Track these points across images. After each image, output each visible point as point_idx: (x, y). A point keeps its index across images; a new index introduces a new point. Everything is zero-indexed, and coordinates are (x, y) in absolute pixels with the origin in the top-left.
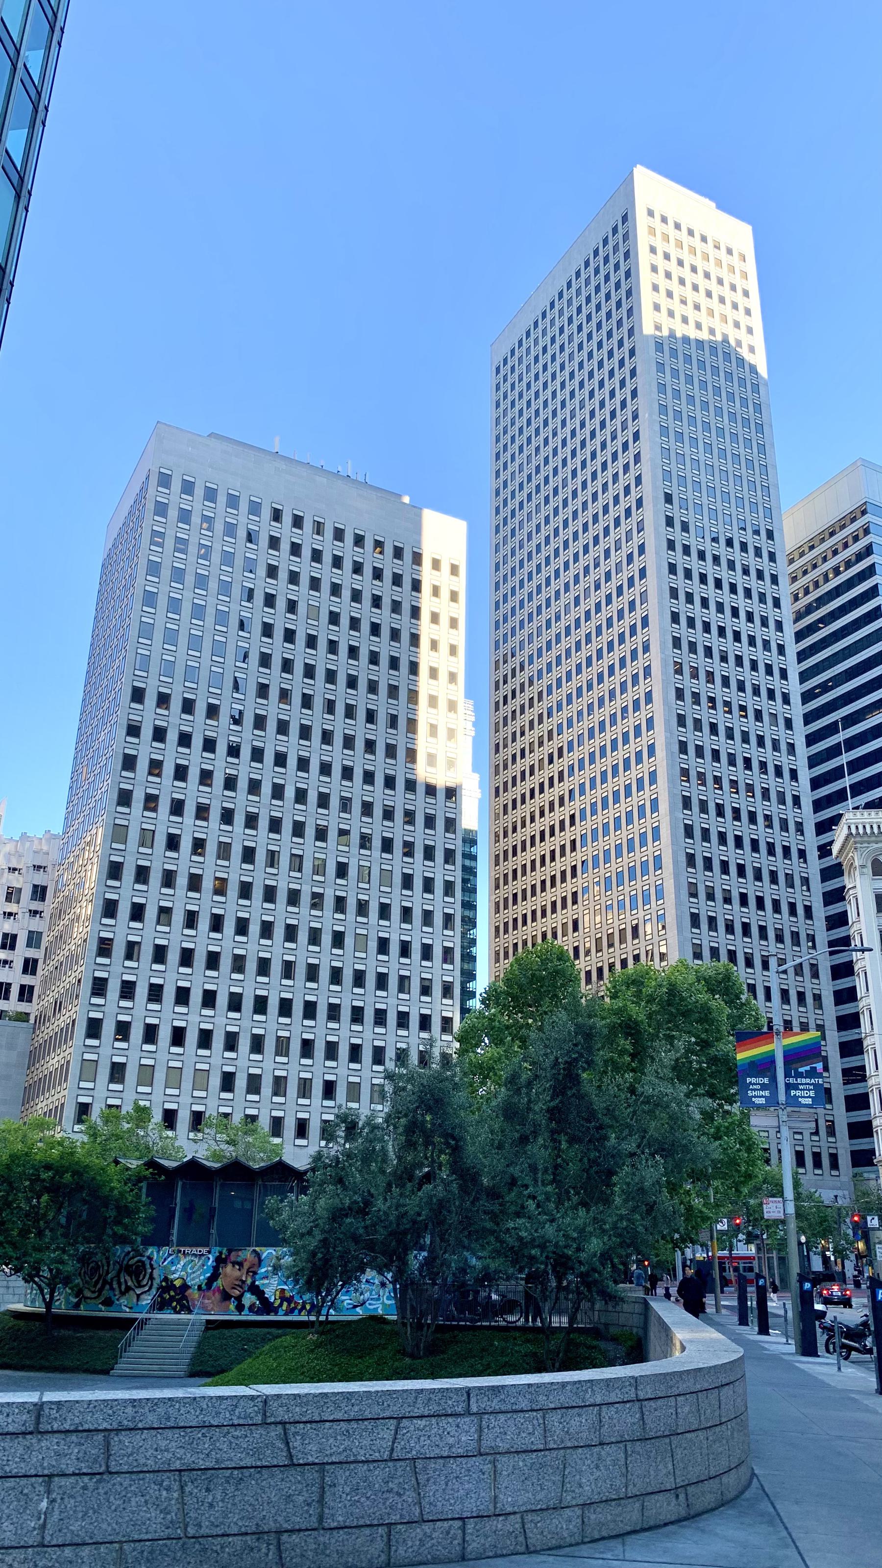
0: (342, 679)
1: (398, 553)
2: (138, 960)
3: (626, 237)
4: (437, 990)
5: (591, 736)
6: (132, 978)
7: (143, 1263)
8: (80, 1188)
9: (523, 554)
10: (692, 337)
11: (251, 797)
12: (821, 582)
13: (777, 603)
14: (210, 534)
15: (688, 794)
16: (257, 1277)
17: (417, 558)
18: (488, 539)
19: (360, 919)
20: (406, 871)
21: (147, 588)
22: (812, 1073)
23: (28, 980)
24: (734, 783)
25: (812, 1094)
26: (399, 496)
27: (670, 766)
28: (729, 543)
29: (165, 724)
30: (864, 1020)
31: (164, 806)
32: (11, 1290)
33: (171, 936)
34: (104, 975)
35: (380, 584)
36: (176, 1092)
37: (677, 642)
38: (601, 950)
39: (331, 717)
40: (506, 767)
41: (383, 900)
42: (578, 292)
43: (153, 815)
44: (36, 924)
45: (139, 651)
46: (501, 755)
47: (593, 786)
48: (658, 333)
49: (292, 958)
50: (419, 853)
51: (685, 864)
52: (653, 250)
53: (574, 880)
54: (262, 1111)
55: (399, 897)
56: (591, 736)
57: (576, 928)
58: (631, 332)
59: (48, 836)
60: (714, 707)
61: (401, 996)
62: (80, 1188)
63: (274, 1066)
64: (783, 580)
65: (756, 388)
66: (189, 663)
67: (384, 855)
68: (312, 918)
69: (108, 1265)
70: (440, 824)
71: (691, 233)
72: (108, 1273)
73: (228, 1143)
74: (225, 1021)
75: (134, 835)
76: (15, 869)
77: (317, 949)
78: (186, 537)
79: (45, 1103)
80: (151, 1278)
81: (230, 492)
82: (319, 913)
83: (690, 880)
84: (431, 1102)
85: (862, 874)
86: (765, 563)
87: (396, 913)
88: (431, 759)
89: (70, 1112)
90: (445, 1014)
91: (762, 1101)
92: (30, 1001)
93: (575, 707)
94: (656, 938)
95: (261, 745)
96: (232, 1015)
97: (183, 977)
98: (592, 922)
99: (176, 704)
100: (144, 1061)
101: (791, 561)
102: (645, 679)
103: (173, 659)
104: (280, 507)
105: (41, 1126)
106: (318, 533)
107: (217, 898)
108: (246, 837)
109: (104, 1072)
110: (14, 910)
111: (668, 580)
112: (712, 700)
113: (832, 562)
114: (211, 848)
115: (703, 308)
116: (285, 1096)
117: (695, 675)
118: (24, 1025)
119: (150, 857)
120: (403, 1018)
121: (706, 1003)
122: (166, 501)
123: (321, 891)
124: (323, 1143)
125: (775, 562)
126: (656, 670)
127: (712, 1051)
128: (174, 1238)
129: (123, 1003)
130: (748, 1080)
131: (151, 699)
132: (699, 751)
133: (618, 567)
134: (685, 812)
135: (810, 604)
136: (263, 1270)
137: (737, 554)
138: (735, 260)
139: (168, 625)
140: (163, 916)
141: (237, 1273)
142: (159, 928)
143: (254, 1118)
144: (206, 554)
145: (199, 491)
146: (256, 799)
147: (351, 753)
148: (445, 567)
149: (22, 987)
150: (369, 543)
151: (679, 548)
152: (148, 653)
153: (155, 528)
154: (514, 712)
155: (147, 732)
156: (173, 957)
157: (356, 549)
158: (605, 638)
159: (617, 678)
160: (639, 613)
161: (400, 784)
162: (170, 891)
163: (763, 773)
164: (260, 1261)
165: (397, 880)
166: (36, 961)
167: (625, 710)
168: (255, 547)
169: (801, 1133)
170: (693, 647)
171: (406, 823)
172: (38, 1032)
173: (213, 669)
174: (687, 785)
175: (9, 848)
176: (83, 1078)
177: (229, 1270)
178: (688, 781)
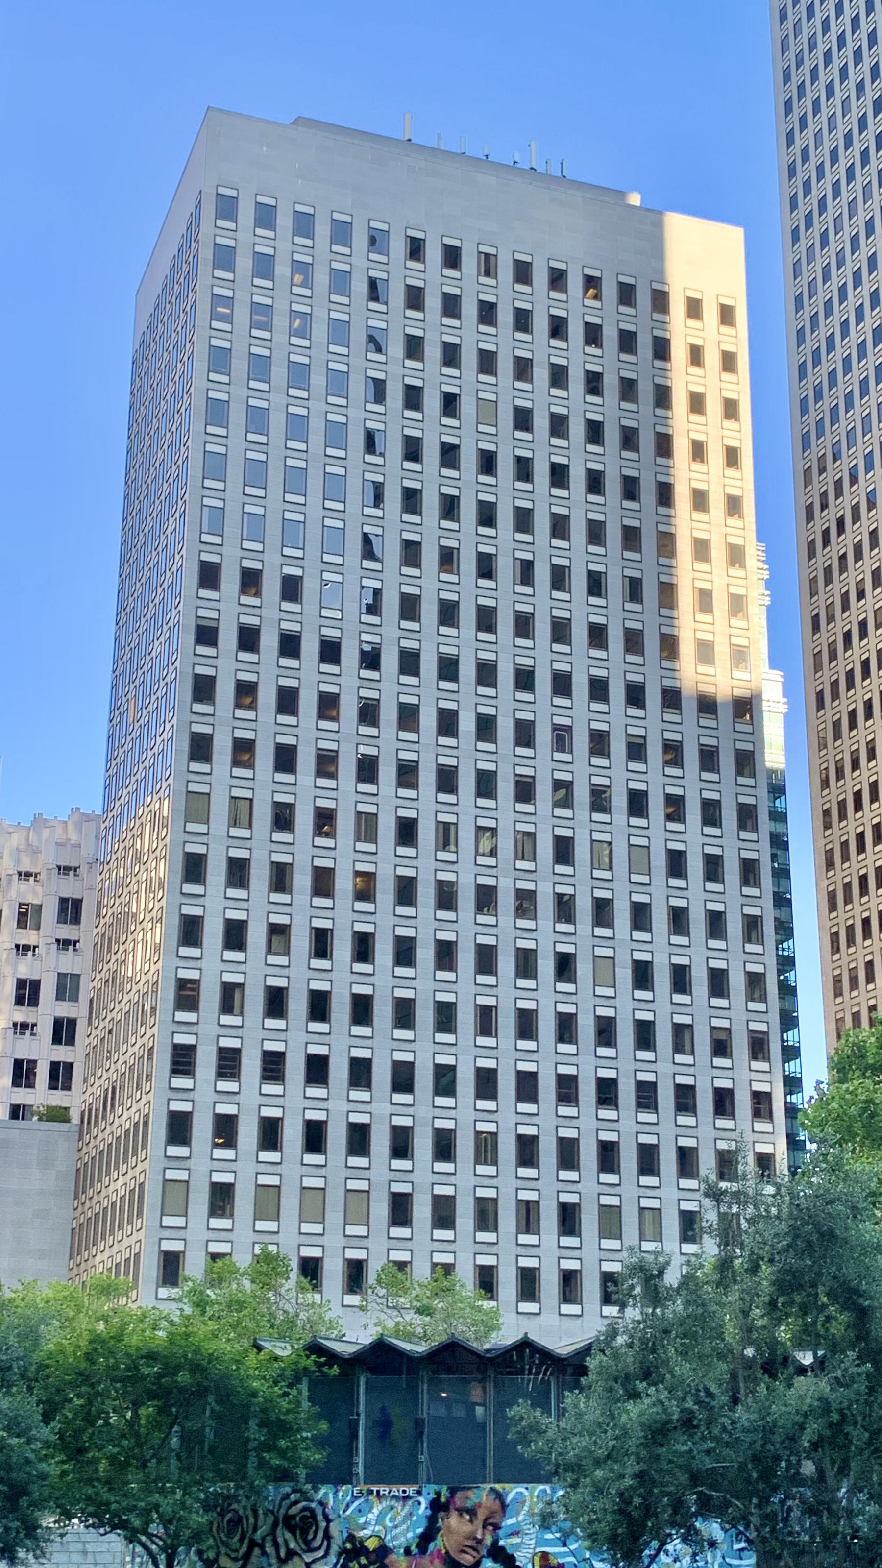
1: (627, 294)
2: (241, 1014)
4: (740, 1046)
6: (235, 1043)
7: (312, 1511)
8: (202, 1392)
9: (841, 276)
11: (403, 735)
14: (307, 292)
16: (501, 1532)
17: (660, 301)
19: (599, 931)
20: (672, 846)
21: (211, 394)
23: (62, 1054)
26: (621, 194)
29: (255, 621)
31: (265, 757)
32: (90, 1558)
33: (291, 972)
34: (189, 1040)
35: (598, 352)
36: (317, 1228)
39: (528, 590)
40: (833, 656)
41: (636, 898)
43: (248, 773)
44: (68, 962)
45: (206, 501)
46: (824, 637)
49: (491, 1001)
50: (693, 813)
54: (461, 1256)
55: (665, 891)
59: (76, 817)
61: (679, 1058)
62: (202, 1392)
63: (474, 1181)
66: (288, 515)
67: (634, 821)
68: (519, 933)
69: (256, 1516)
70: (727, 761)
72: (255, 1529)
73: (419, 1311)
74: (389, 1109)
75: (220, 809)
76: (28, 875)
77: (531, 984)
78: (268, 302)
79: (107, 1253)
80: (327, 1536)
81: (336, 216)
82: (530, 924)
87: (698, 923)
88: (705, 652)
89: (150, 1268)
90: (757, 1087)
92: (69, 1088)
95: (415, 645)
96: (399, 1098)
97: (316, 1038)
99: (271, 586)
100: (263, 1180)
103: (260, 511)
104: (420, 235)
105: (106, 1290)
106: (487, 273)
107: (360, 906)
108: (400, 802)
109: (200, 1200)
110: (32, 942)
114: (345, 823)
116: (496, 1230)
118: (64, 1126)
119: (248, 844)
122: (232, 243)
123: (530, 886)
124: (611, 1310)
128: (360, 1470)
129: (223, 1086)
131: (230, 581)
136: (509, 1522)
139: (250, 454)
140: (275, 939)
141: (467, 1528)
142: (272, 959)
143: (448, 1269)
144: (303, 326)
145: (284, 221)
146: (412, 737)
147: (565, 649)
148: (711, 313)
149: (55, 1067)
150: (575, 283)
152: (220, 504)
153: (217, 291)
154: (843, 558)
155: (228, 637)
156: (298, 1005)
161: (653, 697)
162: (284, 898)
164: (504, 1507)
165: (660, 861)
166: (72, 1023)
168: (383, 308)
171: (667, 763)
172: (87, 1138)
173: (328, 522)
175: (16, 840)
176: (166, 1211)
177: (454, 1522)
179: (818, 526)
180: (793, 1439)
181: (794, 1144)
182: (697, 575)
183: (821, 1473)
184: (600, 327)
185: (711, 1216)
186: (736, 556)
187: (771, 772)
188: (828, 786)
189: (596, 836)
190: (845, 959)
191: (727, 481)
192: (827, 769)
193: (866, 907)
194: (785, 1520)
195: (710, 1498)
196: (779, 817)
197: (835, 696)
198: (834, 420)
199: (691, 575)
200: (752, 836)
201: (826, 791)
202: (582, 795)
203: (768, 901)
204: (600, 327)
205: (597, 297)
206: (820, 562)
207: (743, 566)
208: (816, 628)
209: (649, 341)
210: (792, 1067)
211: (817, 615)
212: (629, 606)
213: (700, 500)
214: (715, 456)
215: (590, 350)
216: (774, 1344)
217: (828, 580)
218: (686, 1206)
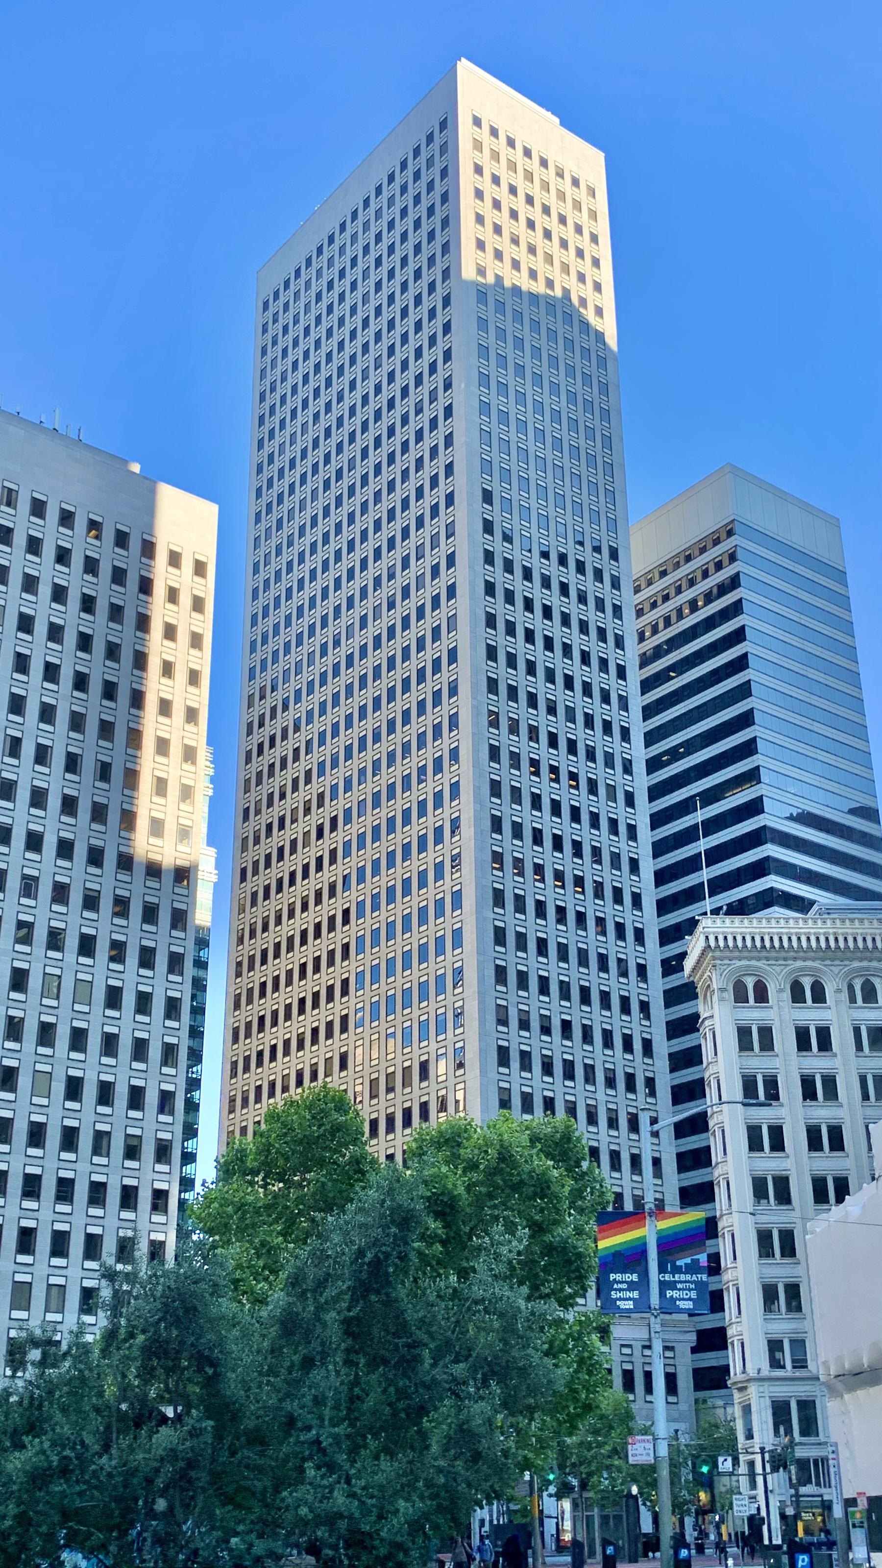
0: (32, 709)
1: (122, 539)
3: (444, 149)
4: (148, 1151)
5: (376, 803)
10: (524, 288)
12: (674, 619)
13: (619, 643)
15: (501, 887)
17: (148, 549)
18: (247, 531)
19: (42, 1050)
22: (694, 1268)
24: (559, 876)
25: (693, 1294)
26: (126, 462)
27: (479, 849)
28: (563, 560)
30: (720, 1193)
37: (492, 685)
38: (376, 1096)
39: (15, 762)
40: (257, 841)
42: (378, 214)
47: (376, 871)
48: (480, 279)
50: (132, 957)
51: (493, 981)
52: (478, 170)
53: (345, 999)
56: (376, 803)
57: (343, 1066)
58: (446, 274)
60: (537, 773)
64: (628, 613)
65: (603, 362)
67: (82, 960)
70: (165, 917)
71: (527, 153)
83: (499, 1002)
84: (181, 1313)
85: (721, 1000)
86: (606, 590)
88: (157, 827)
91: (630, 1305)
93: (355, 764)
94: (452, 1080)
98: (367, 1057)
101: (637, 590)
102: (451, 731)
111: (485, 603)
112: (534, 763)
113: (688, 595)
115: (540, 252)
117: (514, 728)
120: (98, 1192)
121: (544, 1174)
125: (619, 589)
126: (465, 720)
127: (548, 1238)
130: (612, 1277)
132: (517, 831)
133: (420, 582)
134: (497, 910)
135: (659, 646)
137: (571, 576)
138: (582, 195)
147: (41, 813)
148: (188, 566)
150: (80, 523)
151: (499, 562)
154: (272, 766)
157: (61, 529)
158: (399, 674)
159: (414, 729)
160: (445, 644)
163: (596, 862)
165: (99, 994)
167: (422, 770)
169: (630, 1346)
170: (513, 693)
171: (116, 914)
174: (500, 874)
178: (501, 869)
179: (255, 739)
180: (150, 1481)
181: (183, 1234)
182: (157, 765)
183: (171, 1509)
184: (98, 561)
185: (106, 1293)
186: (189, 754)
187: (198, 929)
188: (242, 943)
189: (49, 970)
190: (241, 1083)
191: (188, 696)
192: (243, 929)
193: (261, 1041)
194: (140, 1550)
195: (76, 1532)
196: (200, 964)
197: (255, 872)
198: (275, 660)
199: (152, 765)
200: (178, 979)
201: (240, 947)
202: (40, 935)
203: (185, 1033)
204: (98, 561)
205: (97, 537)
206: (254, 767)
207: (194, 763)
208: (246, 817)
209: (137, 579)
210: (189, 1169)
211: (248, 808)
212: (98, 784)
213: (165, 707)
214: (181, 675)
215: (87, 577)
216: (143, 1399)
217: (259, 782)
218: (88, 1283)
